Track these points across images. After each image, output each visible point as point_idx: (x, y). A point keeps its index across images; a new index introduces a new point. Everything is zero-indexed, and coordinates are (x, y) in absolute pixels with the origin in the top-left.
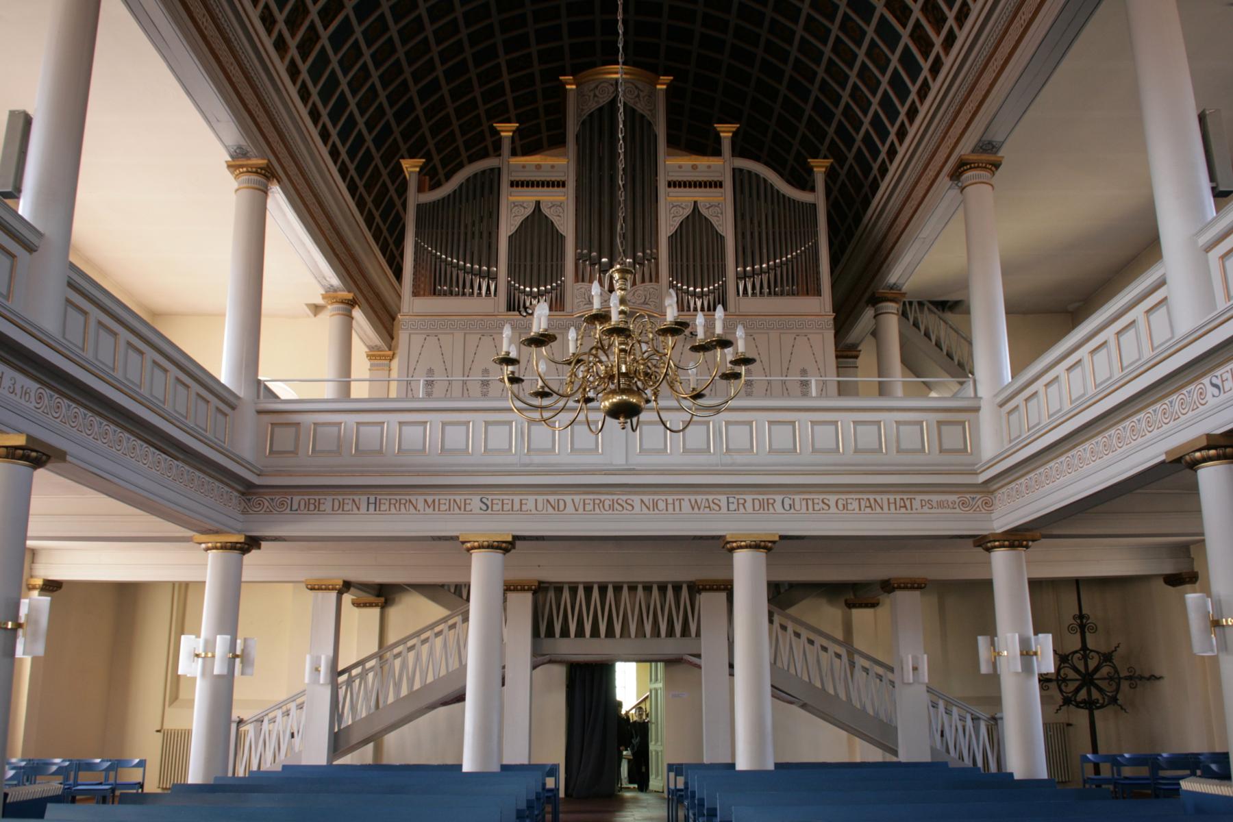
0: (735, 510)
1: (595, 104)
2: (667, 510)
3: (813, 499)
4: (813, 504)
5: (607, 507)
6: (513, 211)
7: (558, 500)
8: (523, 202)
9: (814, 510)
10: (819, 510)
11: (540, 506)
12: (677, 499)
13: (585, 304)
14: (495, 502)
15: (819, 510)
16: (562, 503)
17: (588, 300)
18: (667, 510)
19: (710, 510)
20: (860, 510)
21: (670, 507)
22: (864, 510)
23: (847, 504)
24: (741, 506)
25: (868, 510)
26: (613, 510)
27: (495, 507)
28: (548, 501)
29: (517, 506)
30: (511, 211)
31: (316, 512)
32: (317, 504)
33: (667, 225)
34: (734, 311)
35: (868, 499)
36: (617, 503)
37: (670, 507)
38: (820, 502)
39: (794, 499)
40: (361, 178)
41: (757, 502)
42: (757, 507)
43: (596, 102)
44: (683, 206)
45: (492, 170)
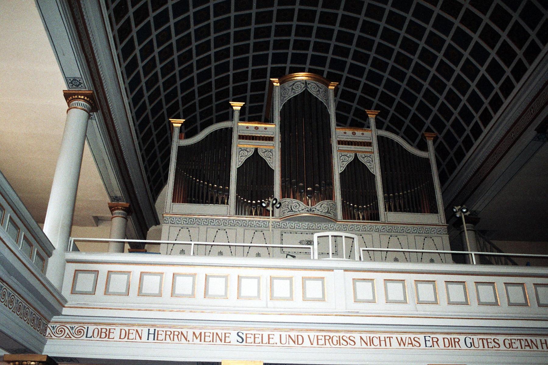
0: (431, 347)
1: (293, 94)
2: (380, 345)
3: (255, 334)
4: (488, 343)
5: (335, 342)
7: (298, 336)
8: (247, 148)
9: (488, 347)
10: (493, 348)
11: (283, 341)
12: (387, 337)
13: (288, 212)
14: (248, 336)
15: (493, 348)
16: (300, 338)
17: (290, 209)
18: (380, 345)
19: (413, 346)
20: (522, 348)
21: (383, 343)
22: (525, 348)
23: (512, 343)
24: (435, 343)
25: (528, 348)
26: (340, 345)
27: (249, 340)
28: (289, 336)
29: (266, 340)
31: (106, 339)
32: (107, 333)
33: (338, 167)
34: (384, 221)
35: (526, 340)
36: (343, 339)
37: (383, 343)
38: (492, 341)
39: (473, 339)
40: (148, 90)
41: (446, 340)
42: (447, 345)
44: (348, 156)
45: (227, 129)
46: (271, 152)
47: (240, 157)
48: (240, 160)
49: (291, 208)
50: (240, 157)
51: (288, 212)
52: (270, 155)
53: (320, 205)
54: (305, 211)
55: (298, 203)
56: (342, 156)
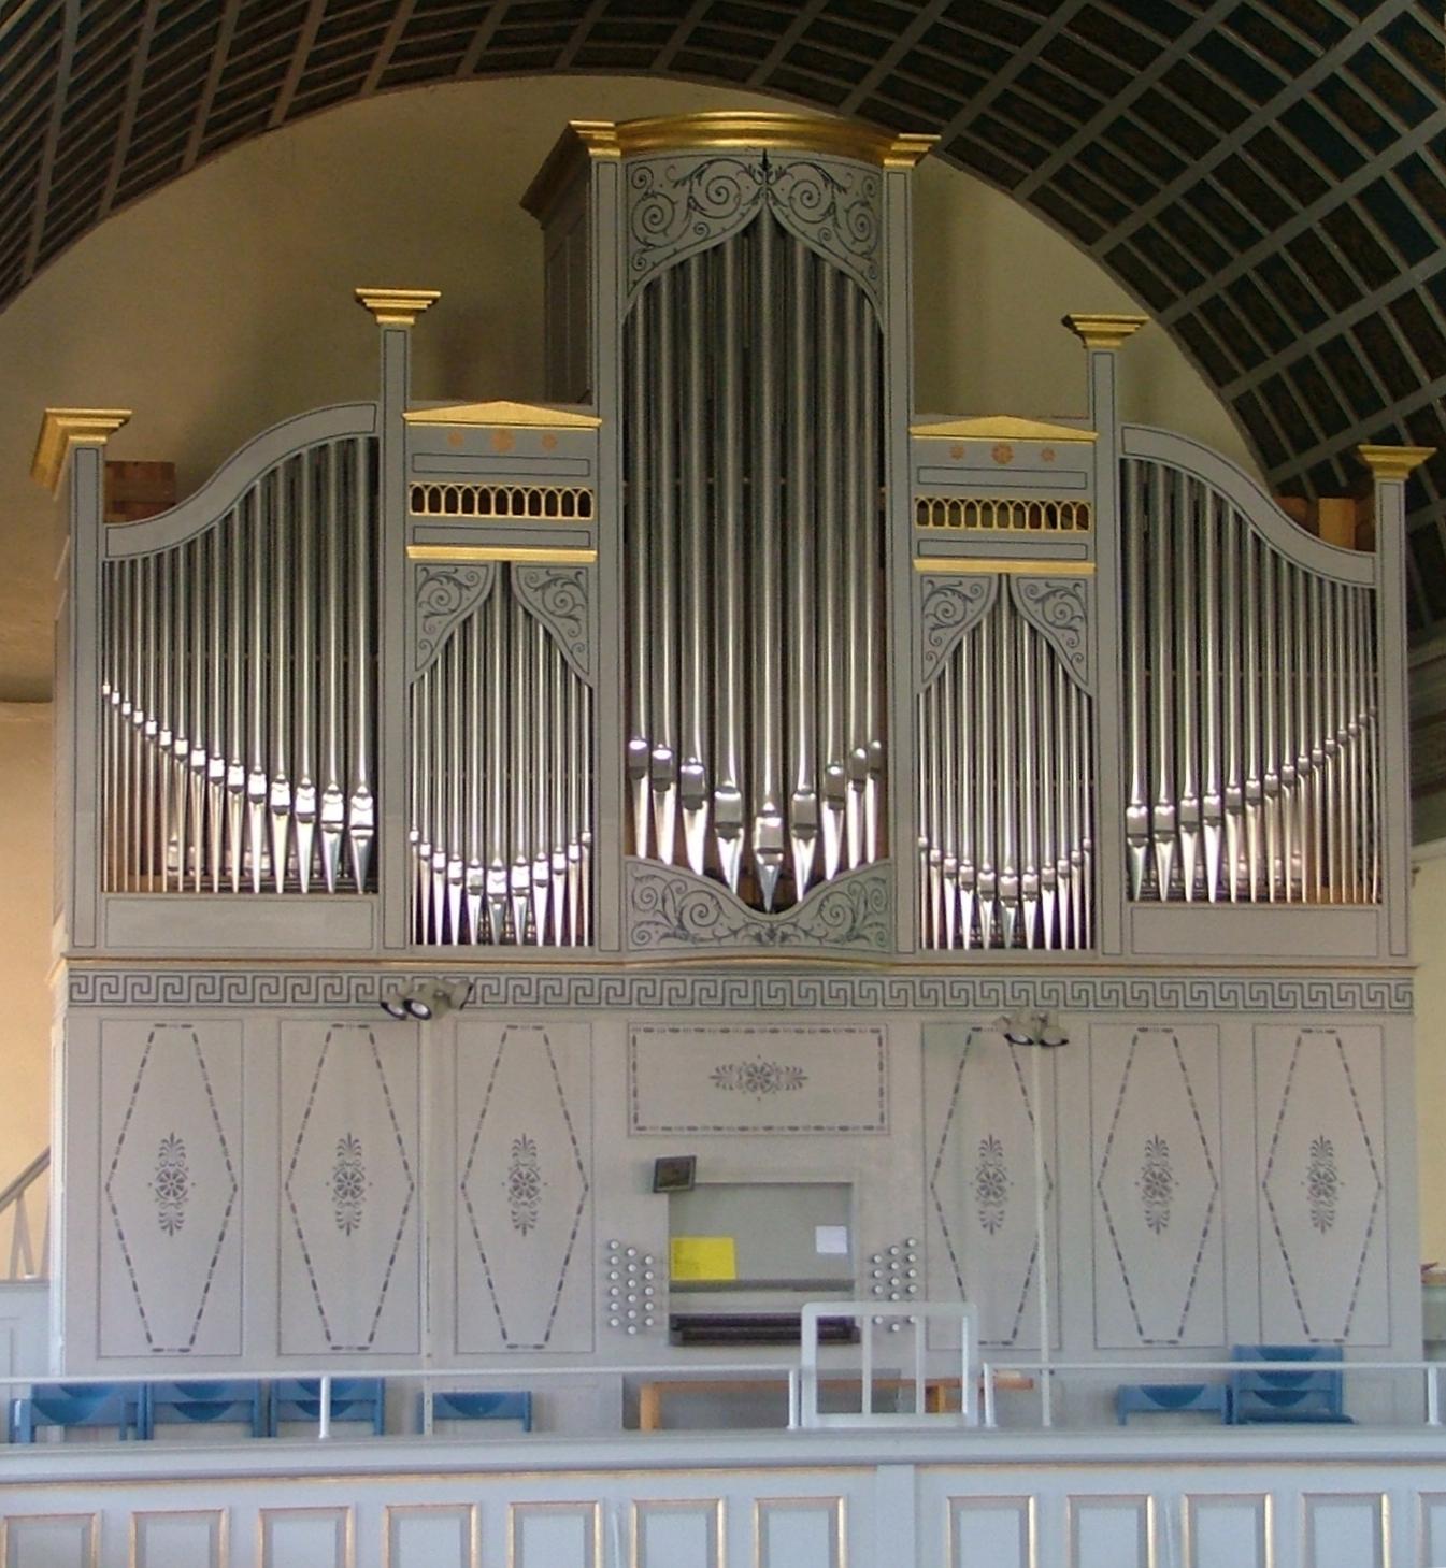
1: (691, 237)
6: (423, 597)
13: (666, 936)
17: (676, 923)
30: (417, 597)
43: (698, 229)
46: (578, 585)
47: (421, 621)
48: (928, 648)
49: (680, 921)
50: (421, 621)
51: (666, 936)
52: (575, 606)
53: (816, 903)
54: (746, 942)
55: (712, 896)
56: (933, 593)
